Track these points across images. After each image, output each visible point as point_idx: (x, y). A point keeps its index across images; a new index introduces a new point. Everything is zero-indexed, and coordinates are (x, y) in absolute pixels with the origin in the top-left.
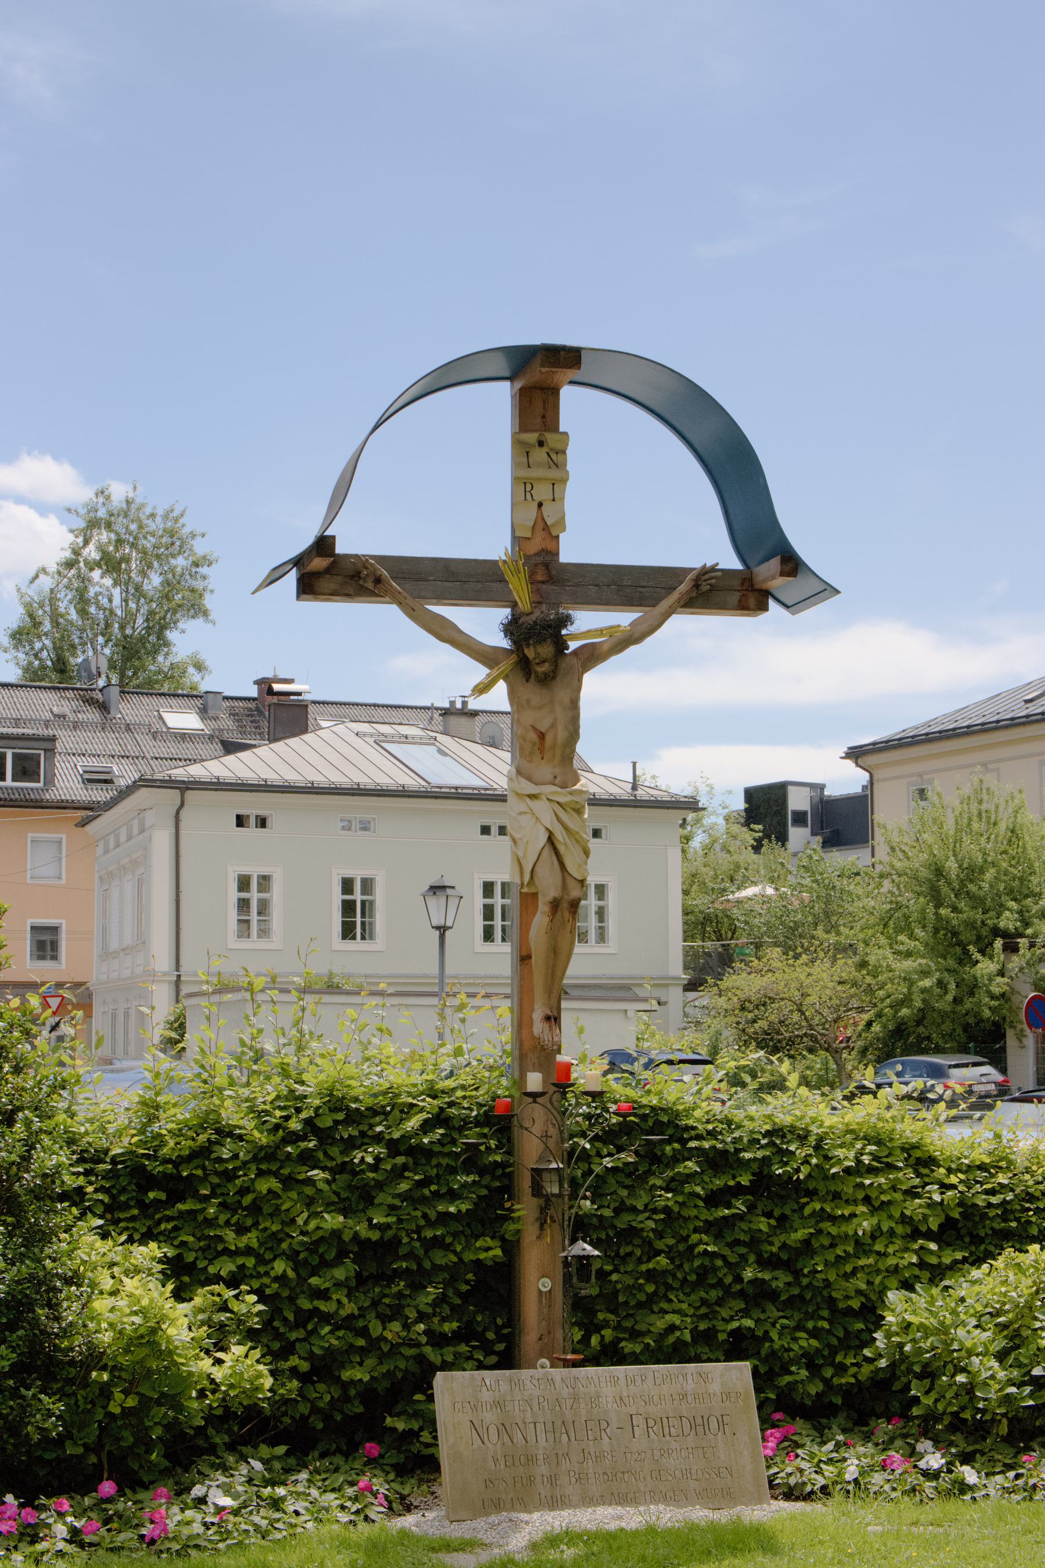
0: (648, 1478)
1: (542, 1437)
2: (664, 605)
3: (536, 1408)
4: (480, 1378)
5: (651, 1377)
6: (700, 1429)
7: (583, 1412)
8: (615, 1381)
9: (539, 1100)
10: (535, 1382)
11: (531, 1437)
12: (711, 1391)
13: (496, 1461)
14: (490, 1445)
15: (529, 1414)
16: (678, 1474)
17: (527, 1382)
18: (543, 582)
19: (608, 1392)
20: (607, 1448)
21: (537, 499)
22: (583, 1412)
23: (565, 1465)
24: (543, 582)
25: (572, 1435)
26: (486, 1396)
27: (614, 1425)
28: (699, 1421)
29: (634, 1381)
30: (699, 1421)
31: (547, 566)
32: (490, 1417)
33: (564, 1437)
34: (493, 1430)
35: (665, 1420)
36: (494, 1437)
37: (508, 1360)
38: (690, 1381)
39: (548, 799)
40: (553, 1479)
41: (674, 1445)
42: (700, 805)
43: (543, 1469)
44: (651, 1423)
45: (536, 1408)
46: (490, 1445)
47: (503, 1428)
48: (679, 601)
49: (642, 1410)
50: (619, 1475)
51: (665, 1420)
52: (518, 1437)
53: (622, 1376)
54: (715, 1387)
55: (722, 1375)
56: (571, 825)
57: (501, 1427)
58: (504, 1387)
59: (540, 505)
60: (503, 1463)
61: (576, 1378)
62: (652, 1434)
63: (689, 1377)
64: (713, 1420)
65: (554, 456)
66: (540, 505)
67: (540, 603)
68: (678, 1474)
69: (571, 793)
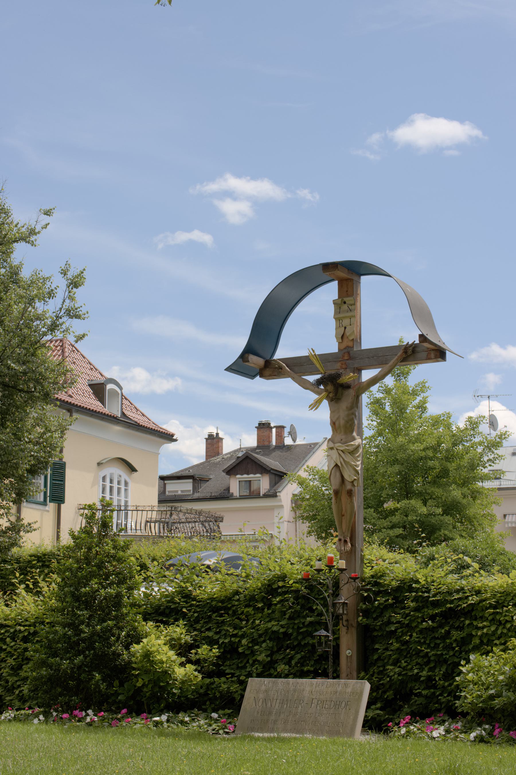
0: (310, 724)
1: (277, 705)
2: (391, 363)
3: (279, 694)
4: (263, 681)
5: (326, 684)
6: (337, 706)
7: (296, 696)
8: (312, 685)
9: (344, 572)
10: (282, 684)
11: (273, 705)
12: (347, 691)
13: (258, 713)
14: (258, 707)
15: (276, 696)
16: (322, 723)
17: (280, 684)
18: (347, 360)
19: (308, 689)
20: (299, 711)
21: (344, 326)
22: (296, 696)
23: (282, 716)
24: (347, 360)
25: (288, 705)
26: (263, 688)
27: (305, 702)
28: (338, 703)
29: (319, 686)
30: (338, 703)
31: (349, 353)
32: (261, 696)
33: (285, 706)
34: (261, 701)
35: (325, 702)
36: (260, 704)
37: (337, 676)
38: (340, 687)
39: (337, 449)
40: (275, 721)
41: (325, 712)
42: (174, 438)
43: (273, 717)
44: (319, 702)
45: (279, 694)
46: (258, 707)
47: (265, 700)
48: (397, 359)
49: (318, 697)
50: (300, 722)
51: (325, 702)
52: (269, 704)
53: (315, 683)
54: (349, 690)
55: (353, 685)
56: (346, 459)
57: (264, 700)
58: (271, 685)
59: (345, 328)
60: (260, 714)
61: (298, 683)
62: (318, 707)
63: (341, 685)
64: (344, 703)
65: (350, 307)
66: (345, 328)
67: (346, 368)
68: (322, 723)
69: (347, 446)
